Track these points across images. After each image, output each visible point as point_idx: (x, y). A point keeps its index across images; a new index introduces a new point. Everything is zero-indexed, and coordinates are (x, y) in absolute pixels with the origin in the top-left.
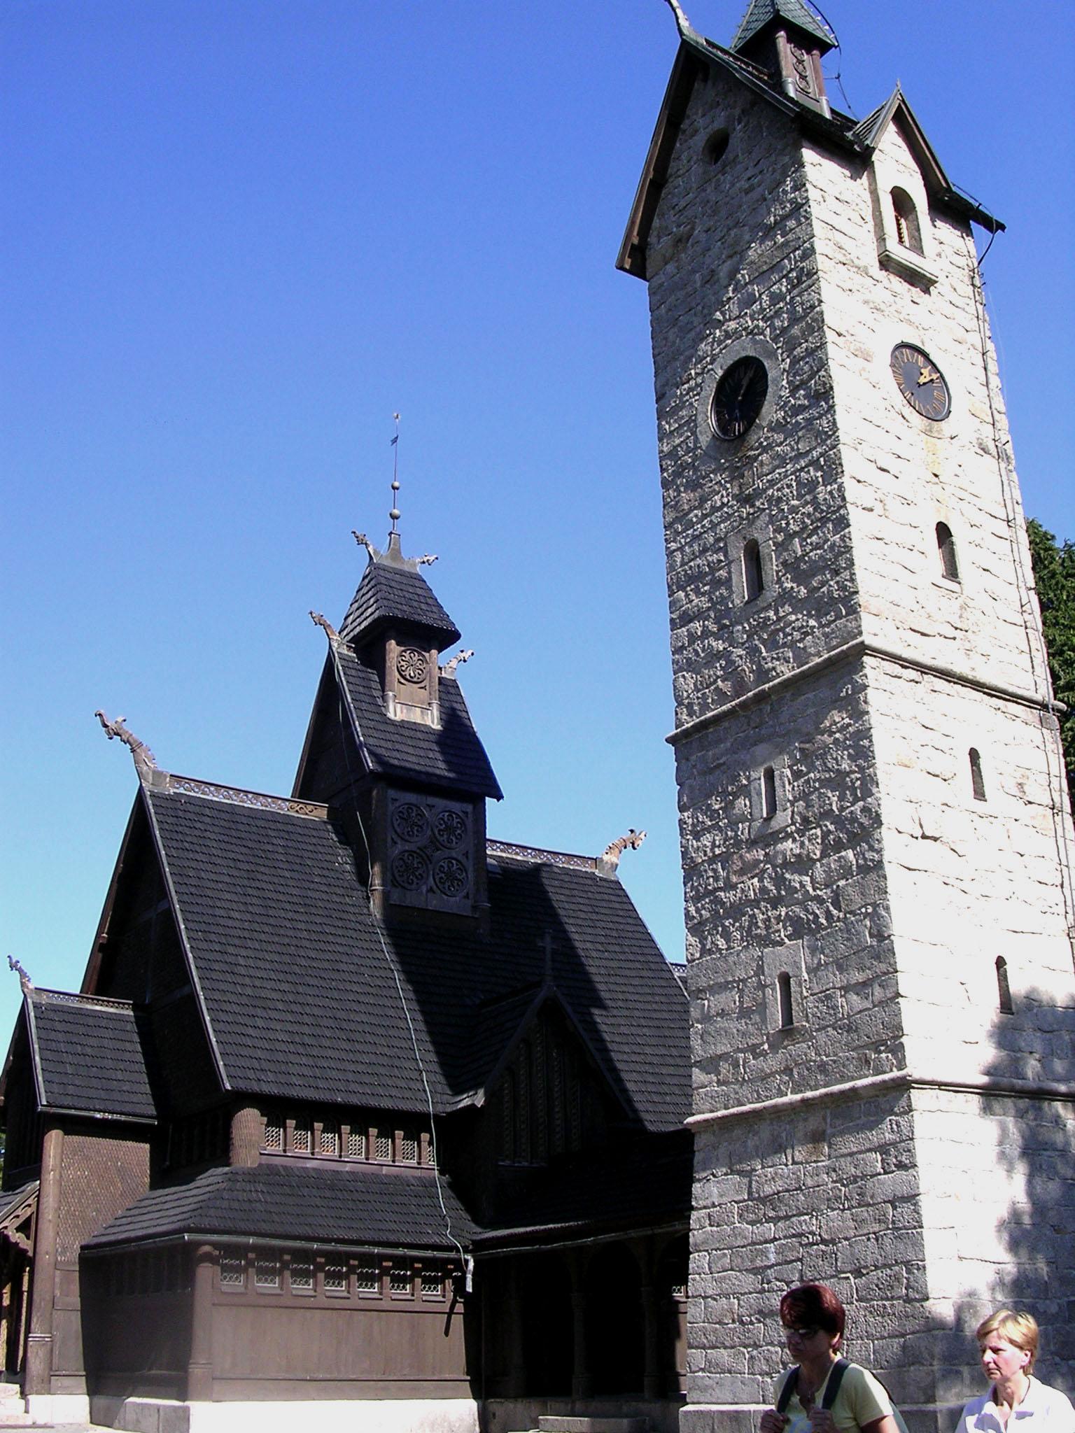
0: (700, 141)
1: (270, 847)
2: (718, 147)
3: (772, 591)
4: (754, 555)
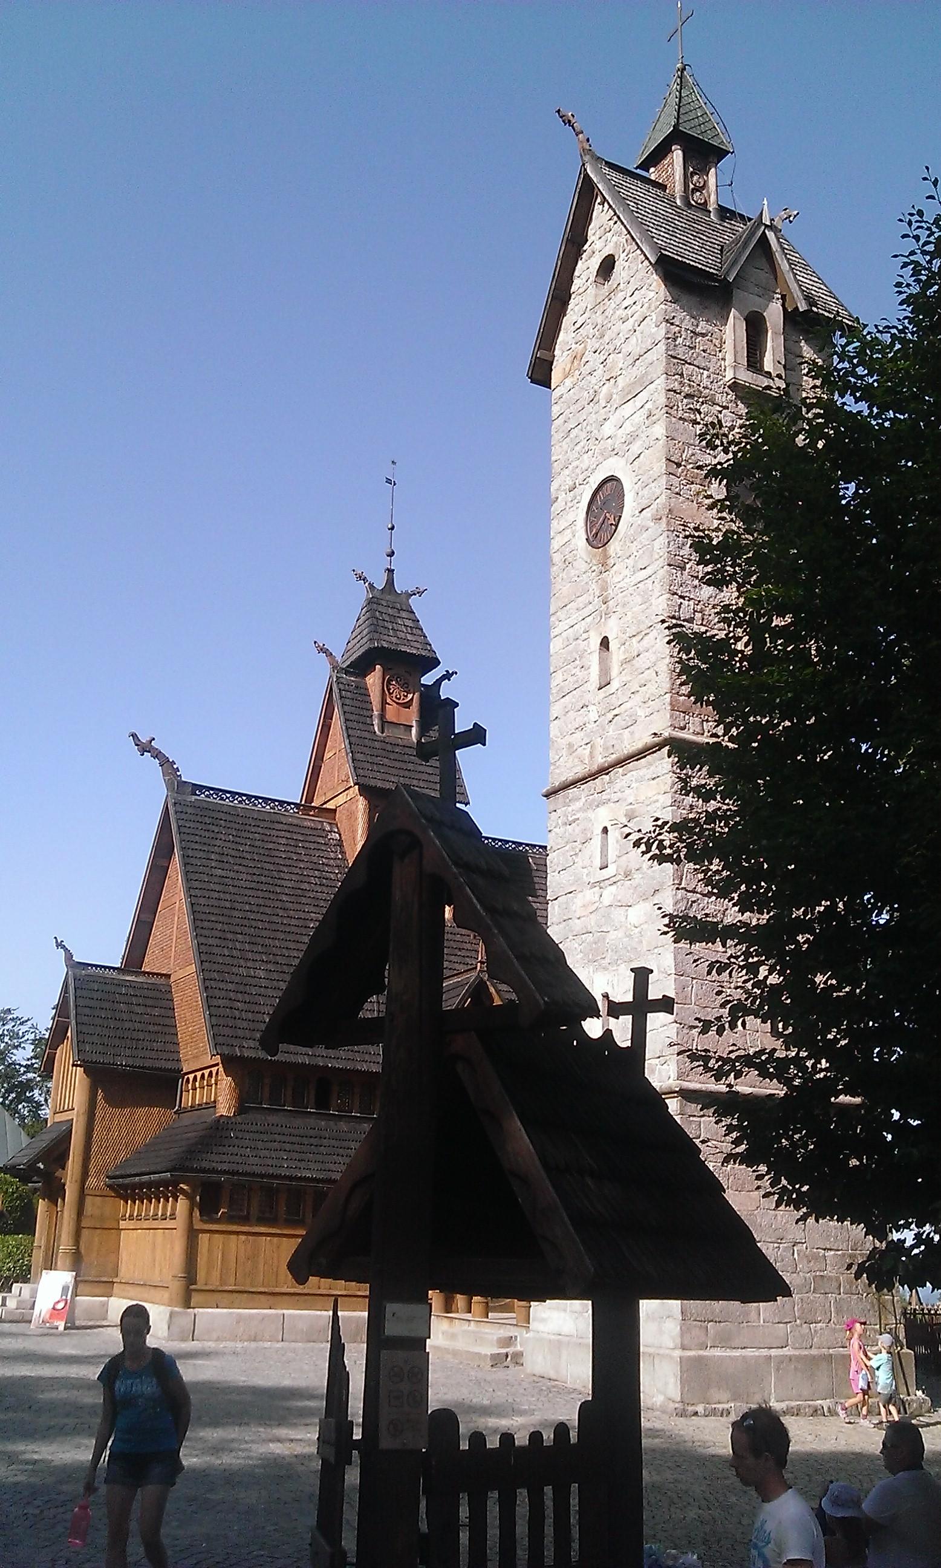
0: (595, 263)
1: (271, 846)
2: (607, 267)
3: (615, 685)
4: (605, 643)
